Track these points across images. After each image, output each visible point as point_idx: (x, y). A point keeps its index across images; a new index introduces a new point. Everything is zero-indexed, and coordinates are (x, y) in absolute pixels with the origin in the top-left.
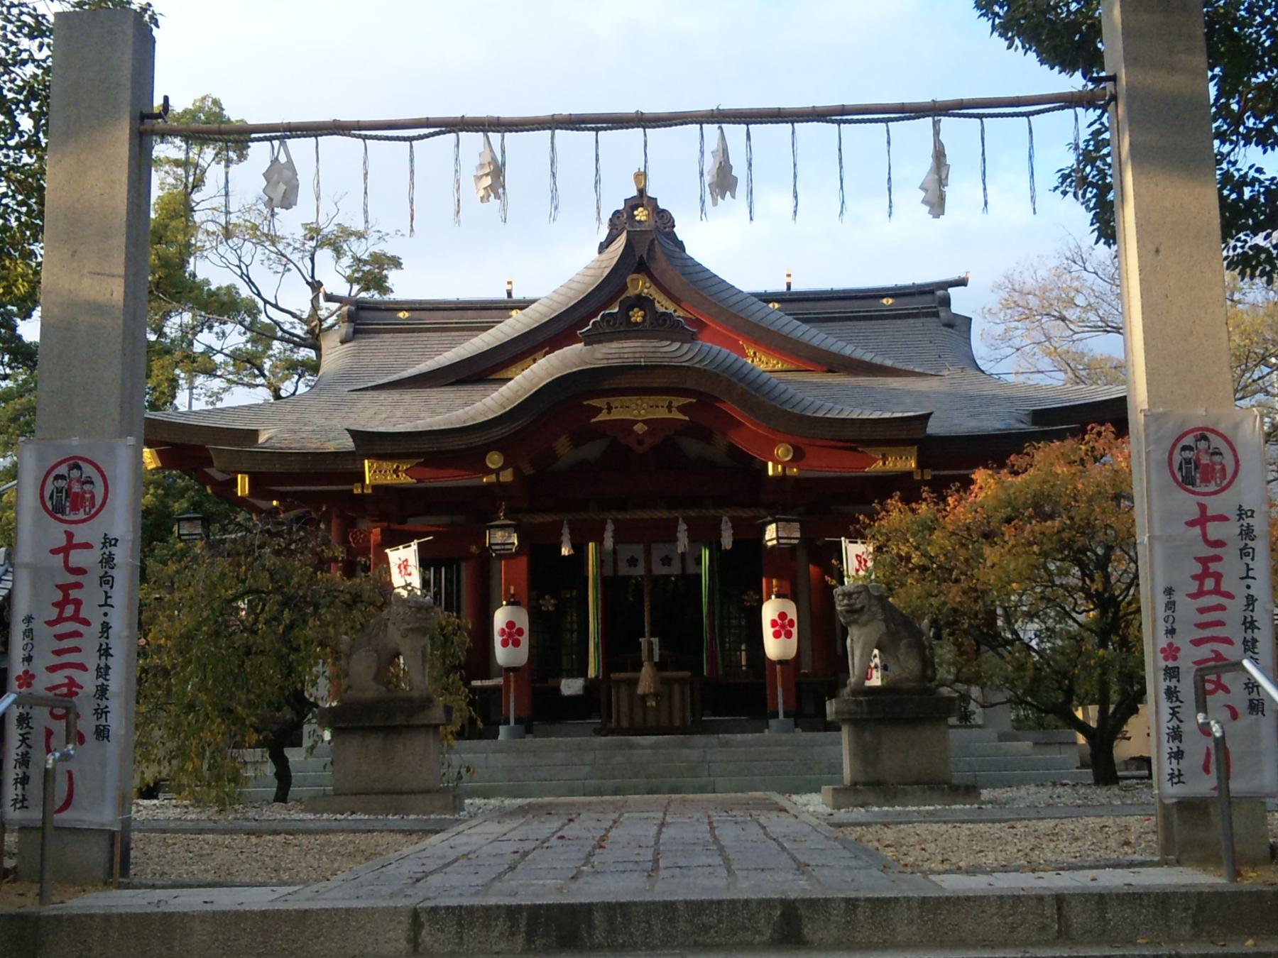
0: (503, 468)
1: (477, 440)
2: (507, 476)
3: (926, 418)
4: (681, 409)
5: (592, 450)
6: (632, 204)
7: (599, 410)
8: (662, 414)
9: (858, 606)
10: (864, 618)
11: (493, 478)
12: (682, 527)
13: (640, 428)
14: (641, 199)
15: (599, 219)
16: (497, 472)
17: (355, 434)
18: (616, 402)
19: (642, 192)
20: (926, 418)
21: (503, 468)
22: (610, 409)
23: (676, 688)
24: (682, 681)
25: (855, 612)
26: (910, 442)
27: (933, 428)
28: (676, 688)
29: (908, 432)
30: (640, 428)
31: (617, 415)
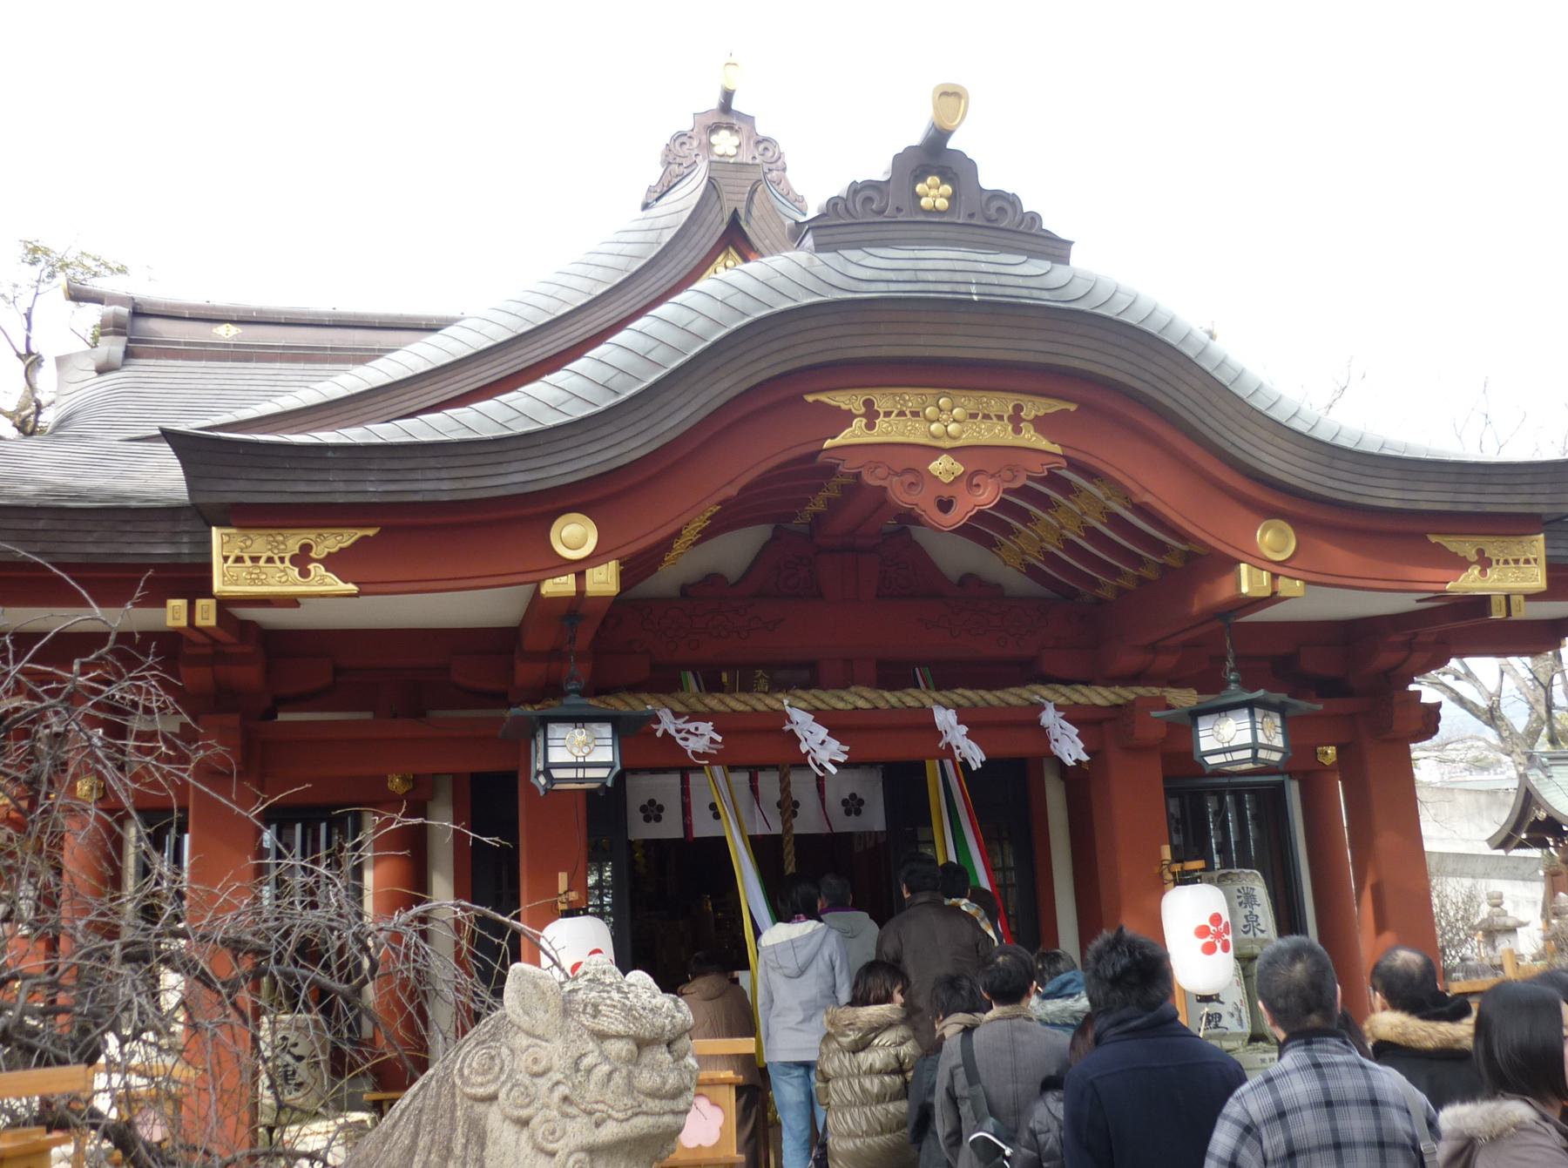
0: (595, 559)
4: (1040, 424)
7: (846, 418)
8: (998, 434)
16: (579, 568)
18: (882, 401)
21: (595, 559)
22: (871, 415)
30: (943, 467)
31: (888, 430)
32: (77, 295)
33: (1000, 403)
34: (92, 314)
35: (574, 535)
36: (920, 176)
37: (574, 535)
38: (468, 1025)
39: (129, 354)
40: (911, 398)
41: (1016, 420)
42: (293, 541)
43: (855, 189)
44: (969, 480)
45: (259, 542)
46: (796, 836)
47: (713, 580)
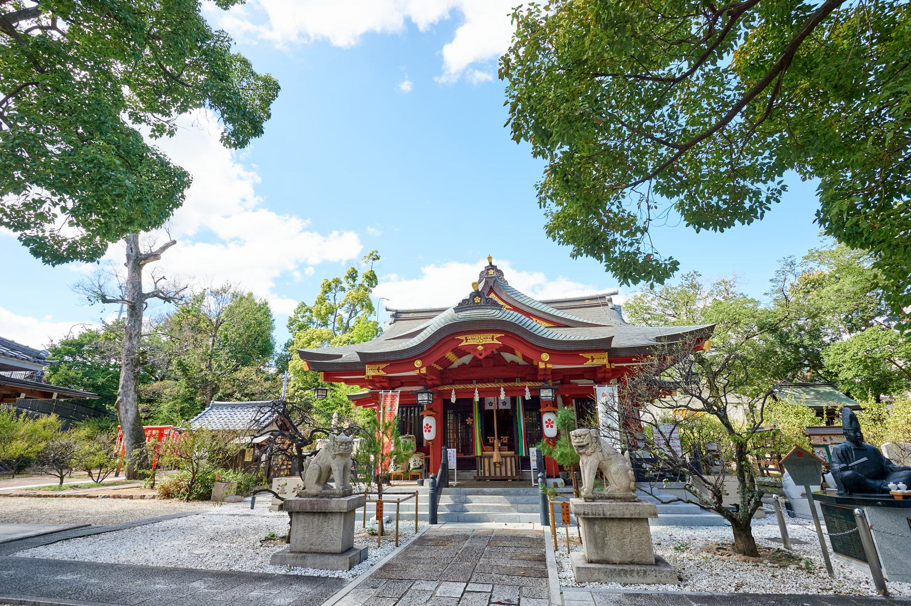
0: (422, 367)
1: (411, 355)
2: (424, 371)
3: (610, 339)
4: (497, 339)
5: (467, 359)
6: (487, 269)
7: (462, 341)
8: (489, 341)
9: (585, 443)
10: (589, 450)
11: (417, 372)
12: (502, 389)
13: (480, 348)
14: (492, 267)
15: (544, 303)
16: (419, 369)
17: (360, 354)
18: (469, 337)
19: (491, 263)
20: (610, 339)
21: (422, 367)
22: (467, 340)
23: (508, 460)
24: (511, 457)
25: (582, 447)
26: (605, 351)
27: (614, 344)
28: (508, 460)
29: (602, 346)
30: (480, 348)
31: (470, 342)
32: (387, 310)
33: (490, 335)
34: (391, 313)
35: (418, 363)
36: (475, 297)
37: (418, 363)
38: (576, 426)
39: (395, 321)
40: (474, 336)
41: (378, 369)
42: (377, 366)
43: (463, 301)
44: (485, 350)
45: (373, 367)
46: (592, 391)
47: (464, 364)
